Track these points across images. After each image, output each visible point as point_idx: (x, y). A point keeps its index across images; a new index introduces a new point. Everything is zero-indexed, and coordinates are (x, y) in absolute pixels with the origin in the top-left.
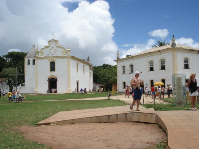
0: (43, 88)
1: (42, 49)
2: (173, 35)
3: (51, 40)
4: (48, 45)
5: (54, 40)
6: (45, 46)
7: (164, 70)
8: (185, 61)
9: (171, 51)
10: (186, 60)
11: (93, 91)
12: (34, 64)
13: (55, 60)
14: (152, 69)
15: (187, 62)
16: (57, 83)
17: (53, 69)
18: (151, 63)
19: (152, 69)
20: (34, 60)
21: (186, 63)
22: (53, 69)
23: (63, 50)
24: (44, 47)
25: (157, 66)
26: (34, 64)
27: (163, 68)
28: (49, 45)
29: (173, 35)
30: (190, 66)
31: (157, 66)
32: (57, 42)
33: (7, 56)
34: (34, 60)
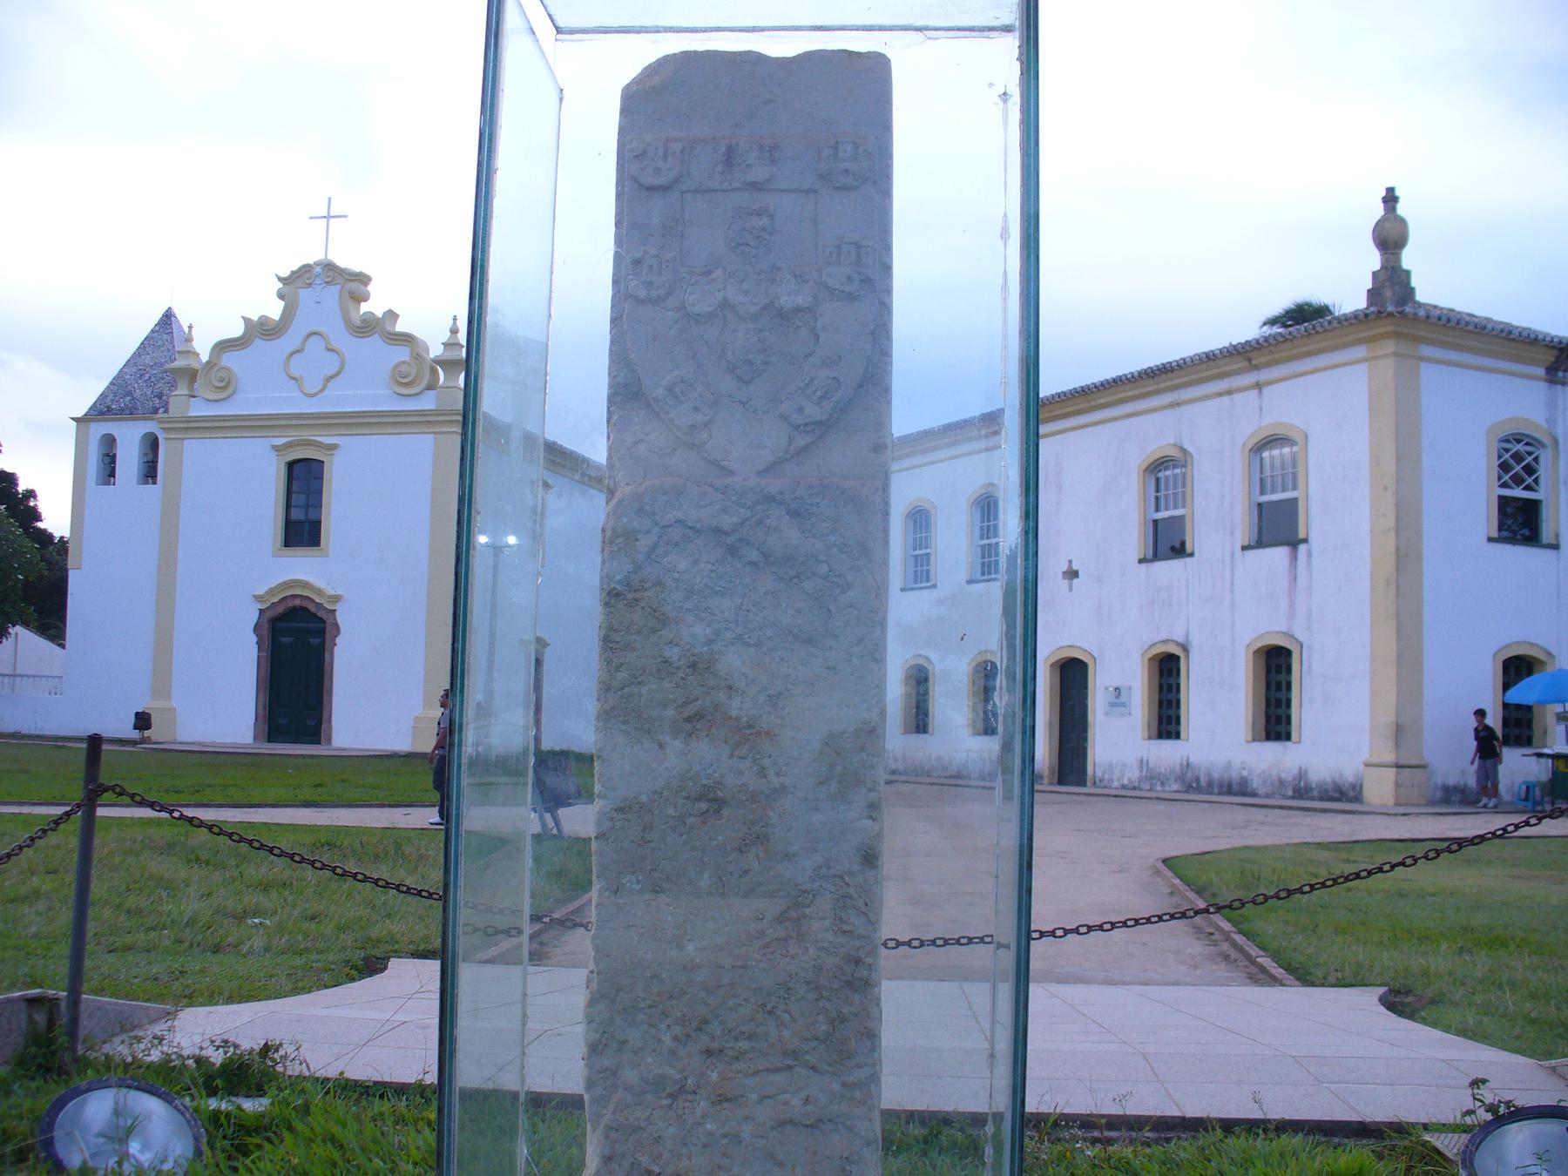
0: (220, 706)
1: (223, 347)
2: (1390, 191)
3: (306, 269)
4: (275, 310)
5: (329, 267)
6: (247, 321)
7: (1279, 554)
8: (1504, 467)
9: (1361, 351)
10: (1517, 457)
11: (101, 1135)
12: (150, 473)
13: (333, 447)
14: (1167, 542)
15: (1530, 470)
16: (337, 650)
17: (302, 530)
18: (1165, 473)
19: (1167, 542)
20: (152, 444)
21: (1517, 480)
22: (302, 530)
23: (403, 354)
24: (237, 330)
25: (1218, 506)
26: (150, 473)
27: (1277, 526)
28: (288, 314)
29: (1390, 191)
30: (1564, 513)
31: (1218, 506)
32: (353, 286)
33: (1407, 293)
34: (152, 444)
